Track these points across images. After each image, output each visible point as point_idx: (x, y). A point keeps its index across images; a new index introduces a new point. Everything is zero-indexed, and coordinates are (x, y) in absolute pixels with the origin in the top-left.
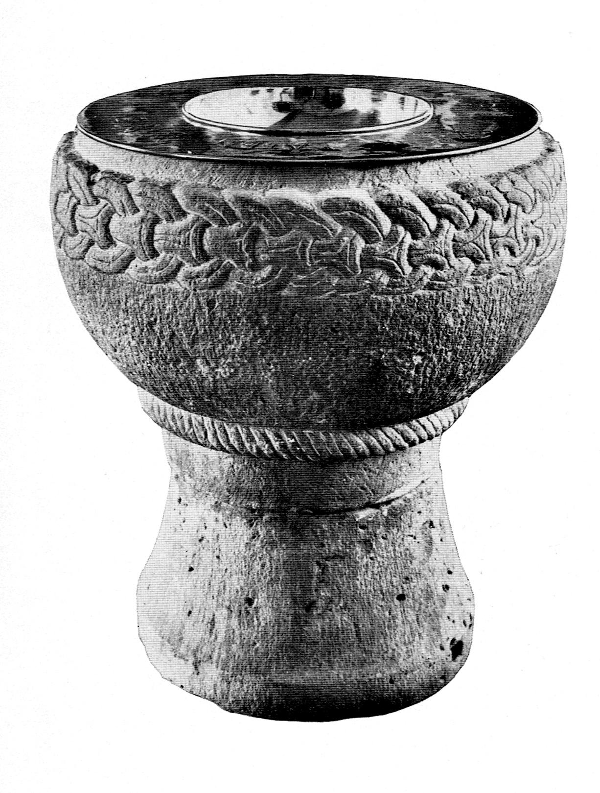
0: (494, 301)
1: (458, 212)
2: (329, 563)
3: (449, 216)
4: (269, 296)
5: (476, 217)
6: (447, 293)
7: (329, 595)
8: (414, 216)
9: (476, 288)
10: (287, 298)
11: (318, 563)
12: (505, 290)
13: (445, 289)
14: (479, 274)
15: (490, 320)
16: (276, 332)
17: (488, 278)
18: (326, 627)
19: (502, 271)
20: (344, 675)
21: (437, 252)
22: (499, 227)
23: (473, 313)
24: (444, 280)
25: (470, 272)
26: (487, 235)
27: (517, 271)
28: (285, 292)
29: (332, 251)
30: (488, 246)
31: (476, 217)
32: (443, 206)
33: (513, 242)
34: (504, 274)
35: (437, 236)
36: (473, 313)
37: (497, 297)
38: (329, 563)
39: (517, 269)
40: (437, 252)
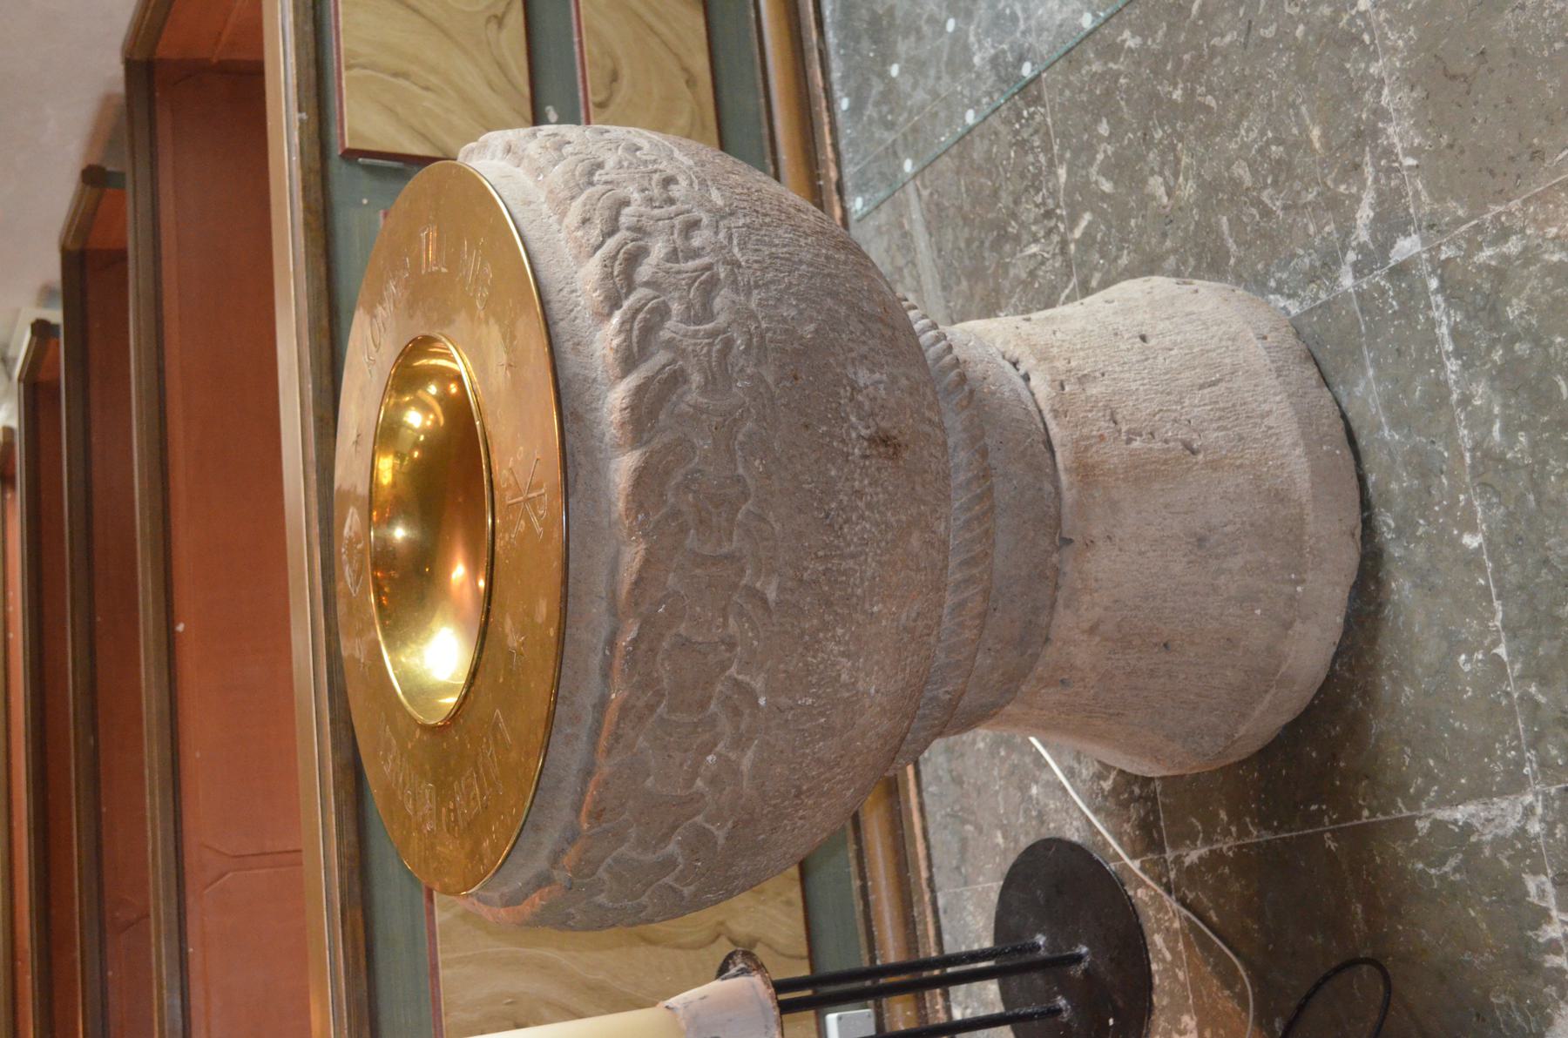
0: (772, 256)
1: (641, 316)
2: (1124, 428)
3: (649, 330)
4: (775, 619)
5: (647, 284)
6: (770, 334)
7: (1169, 426)
8: (655, 385)
9: (757, 286)
10: (781, 589)
11: (1129, 441)
12: (754, 238)
13: (762, 337)
14: (735, 282)
15: (801, 262)
16: (829, 604)
17: (740, 266)
18: (1215, 425)
19: (725, 242)
20: (1275, 394)
21: (709, 352)
22: (658, 249)
23: (794, 290)
24: (751, 340)
25: (735, 297)
26: (676, 267)
27: (723, 218)
28: (772, 595)
29: (678, 486)
30: (691, 264)
31: (647, 284)
32: (635, 340)
33: (677, 221)
34: (730, 238)
35: (684, 350)
36: (794, 290)
37: (766, 250)
38: (1124, 428)
39: (719, 215)
40: (709, 352)
